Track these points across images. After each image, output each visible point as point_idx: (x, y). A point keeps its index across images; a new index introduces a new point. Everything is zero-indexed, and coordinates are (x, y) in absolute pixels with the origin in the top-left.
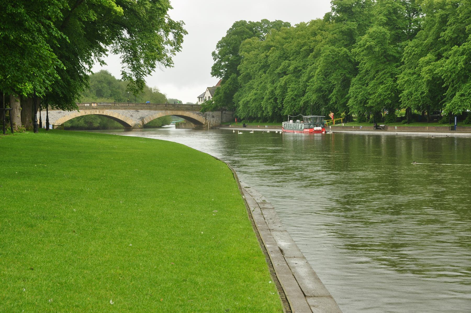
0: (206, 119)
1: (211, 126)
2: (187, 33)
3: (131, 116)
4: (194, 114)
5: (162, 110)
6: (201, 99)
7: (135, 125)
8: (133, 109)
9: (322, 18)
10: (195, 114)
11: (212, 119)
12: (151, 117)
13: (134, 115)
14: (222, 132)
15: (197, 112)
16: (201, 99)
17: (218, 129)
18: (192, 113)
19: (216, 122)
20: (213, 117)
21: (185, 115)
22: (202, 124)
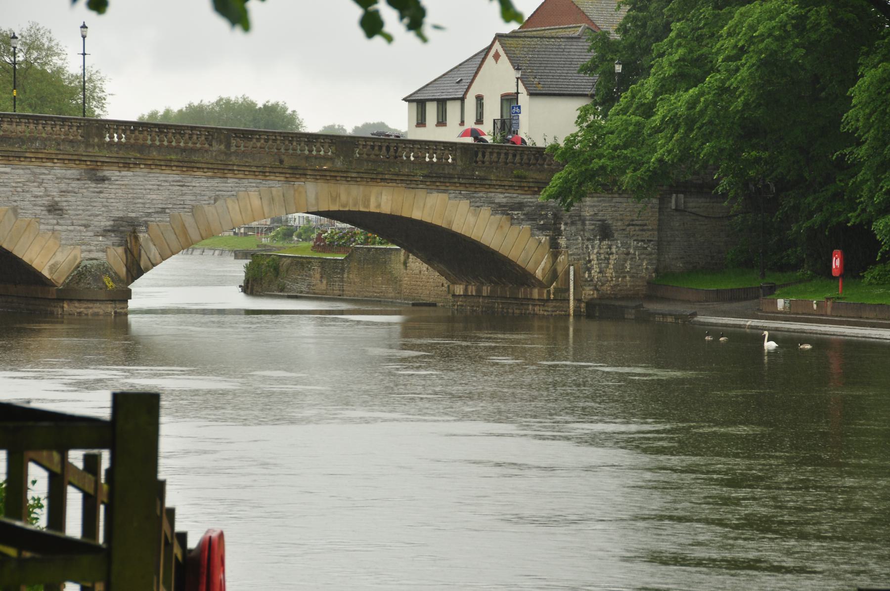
0: (554, 246)
1: (588, 293)
2: (246, 27)
3: (54, 209)
4: (476, 206)
5: (263, 172)
6: (431, 110)
7: (80, 274)
8: (68, 160)
9: (260, 105)
10: (485, 212)
11: (595, 250)
12: (188, 220)
13: (73, 204)
14: (676, 342)
15: (500, 198)
16: (431, 110)
17: (645, 318)
18: (464, 204)
19: (620, 270)
20: (605, 232)
21: (417, 215)
22: (520, 277)
